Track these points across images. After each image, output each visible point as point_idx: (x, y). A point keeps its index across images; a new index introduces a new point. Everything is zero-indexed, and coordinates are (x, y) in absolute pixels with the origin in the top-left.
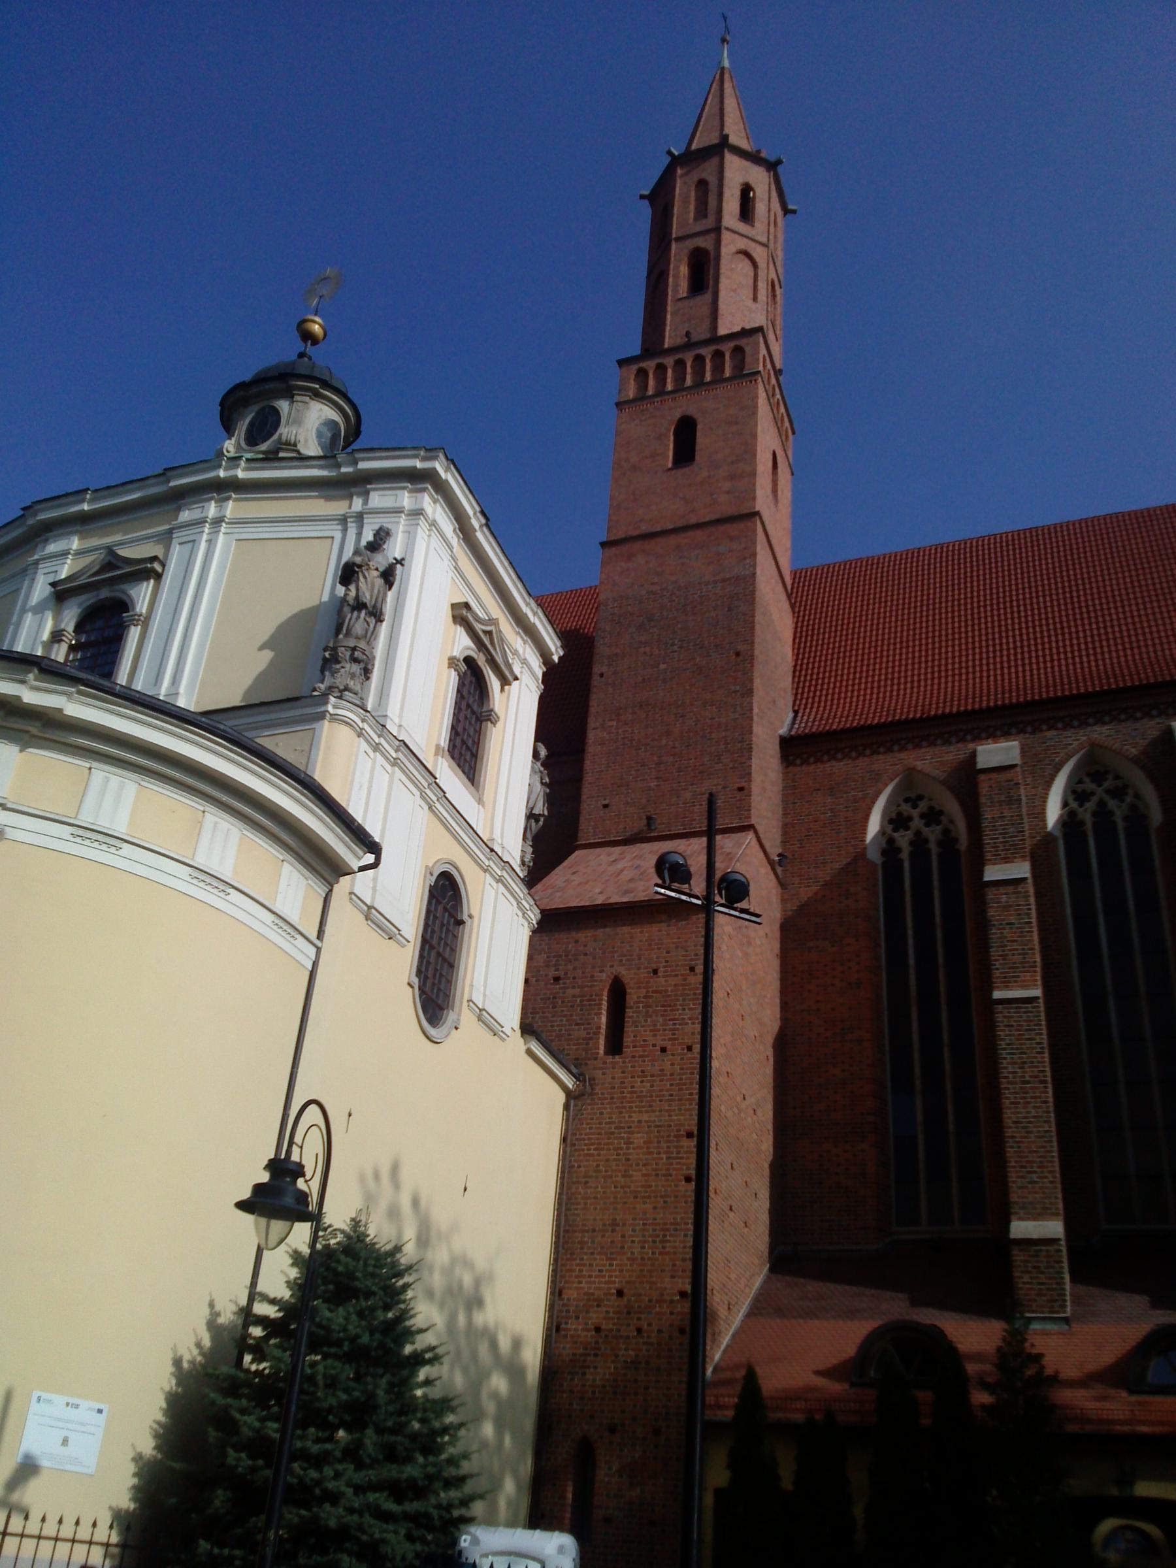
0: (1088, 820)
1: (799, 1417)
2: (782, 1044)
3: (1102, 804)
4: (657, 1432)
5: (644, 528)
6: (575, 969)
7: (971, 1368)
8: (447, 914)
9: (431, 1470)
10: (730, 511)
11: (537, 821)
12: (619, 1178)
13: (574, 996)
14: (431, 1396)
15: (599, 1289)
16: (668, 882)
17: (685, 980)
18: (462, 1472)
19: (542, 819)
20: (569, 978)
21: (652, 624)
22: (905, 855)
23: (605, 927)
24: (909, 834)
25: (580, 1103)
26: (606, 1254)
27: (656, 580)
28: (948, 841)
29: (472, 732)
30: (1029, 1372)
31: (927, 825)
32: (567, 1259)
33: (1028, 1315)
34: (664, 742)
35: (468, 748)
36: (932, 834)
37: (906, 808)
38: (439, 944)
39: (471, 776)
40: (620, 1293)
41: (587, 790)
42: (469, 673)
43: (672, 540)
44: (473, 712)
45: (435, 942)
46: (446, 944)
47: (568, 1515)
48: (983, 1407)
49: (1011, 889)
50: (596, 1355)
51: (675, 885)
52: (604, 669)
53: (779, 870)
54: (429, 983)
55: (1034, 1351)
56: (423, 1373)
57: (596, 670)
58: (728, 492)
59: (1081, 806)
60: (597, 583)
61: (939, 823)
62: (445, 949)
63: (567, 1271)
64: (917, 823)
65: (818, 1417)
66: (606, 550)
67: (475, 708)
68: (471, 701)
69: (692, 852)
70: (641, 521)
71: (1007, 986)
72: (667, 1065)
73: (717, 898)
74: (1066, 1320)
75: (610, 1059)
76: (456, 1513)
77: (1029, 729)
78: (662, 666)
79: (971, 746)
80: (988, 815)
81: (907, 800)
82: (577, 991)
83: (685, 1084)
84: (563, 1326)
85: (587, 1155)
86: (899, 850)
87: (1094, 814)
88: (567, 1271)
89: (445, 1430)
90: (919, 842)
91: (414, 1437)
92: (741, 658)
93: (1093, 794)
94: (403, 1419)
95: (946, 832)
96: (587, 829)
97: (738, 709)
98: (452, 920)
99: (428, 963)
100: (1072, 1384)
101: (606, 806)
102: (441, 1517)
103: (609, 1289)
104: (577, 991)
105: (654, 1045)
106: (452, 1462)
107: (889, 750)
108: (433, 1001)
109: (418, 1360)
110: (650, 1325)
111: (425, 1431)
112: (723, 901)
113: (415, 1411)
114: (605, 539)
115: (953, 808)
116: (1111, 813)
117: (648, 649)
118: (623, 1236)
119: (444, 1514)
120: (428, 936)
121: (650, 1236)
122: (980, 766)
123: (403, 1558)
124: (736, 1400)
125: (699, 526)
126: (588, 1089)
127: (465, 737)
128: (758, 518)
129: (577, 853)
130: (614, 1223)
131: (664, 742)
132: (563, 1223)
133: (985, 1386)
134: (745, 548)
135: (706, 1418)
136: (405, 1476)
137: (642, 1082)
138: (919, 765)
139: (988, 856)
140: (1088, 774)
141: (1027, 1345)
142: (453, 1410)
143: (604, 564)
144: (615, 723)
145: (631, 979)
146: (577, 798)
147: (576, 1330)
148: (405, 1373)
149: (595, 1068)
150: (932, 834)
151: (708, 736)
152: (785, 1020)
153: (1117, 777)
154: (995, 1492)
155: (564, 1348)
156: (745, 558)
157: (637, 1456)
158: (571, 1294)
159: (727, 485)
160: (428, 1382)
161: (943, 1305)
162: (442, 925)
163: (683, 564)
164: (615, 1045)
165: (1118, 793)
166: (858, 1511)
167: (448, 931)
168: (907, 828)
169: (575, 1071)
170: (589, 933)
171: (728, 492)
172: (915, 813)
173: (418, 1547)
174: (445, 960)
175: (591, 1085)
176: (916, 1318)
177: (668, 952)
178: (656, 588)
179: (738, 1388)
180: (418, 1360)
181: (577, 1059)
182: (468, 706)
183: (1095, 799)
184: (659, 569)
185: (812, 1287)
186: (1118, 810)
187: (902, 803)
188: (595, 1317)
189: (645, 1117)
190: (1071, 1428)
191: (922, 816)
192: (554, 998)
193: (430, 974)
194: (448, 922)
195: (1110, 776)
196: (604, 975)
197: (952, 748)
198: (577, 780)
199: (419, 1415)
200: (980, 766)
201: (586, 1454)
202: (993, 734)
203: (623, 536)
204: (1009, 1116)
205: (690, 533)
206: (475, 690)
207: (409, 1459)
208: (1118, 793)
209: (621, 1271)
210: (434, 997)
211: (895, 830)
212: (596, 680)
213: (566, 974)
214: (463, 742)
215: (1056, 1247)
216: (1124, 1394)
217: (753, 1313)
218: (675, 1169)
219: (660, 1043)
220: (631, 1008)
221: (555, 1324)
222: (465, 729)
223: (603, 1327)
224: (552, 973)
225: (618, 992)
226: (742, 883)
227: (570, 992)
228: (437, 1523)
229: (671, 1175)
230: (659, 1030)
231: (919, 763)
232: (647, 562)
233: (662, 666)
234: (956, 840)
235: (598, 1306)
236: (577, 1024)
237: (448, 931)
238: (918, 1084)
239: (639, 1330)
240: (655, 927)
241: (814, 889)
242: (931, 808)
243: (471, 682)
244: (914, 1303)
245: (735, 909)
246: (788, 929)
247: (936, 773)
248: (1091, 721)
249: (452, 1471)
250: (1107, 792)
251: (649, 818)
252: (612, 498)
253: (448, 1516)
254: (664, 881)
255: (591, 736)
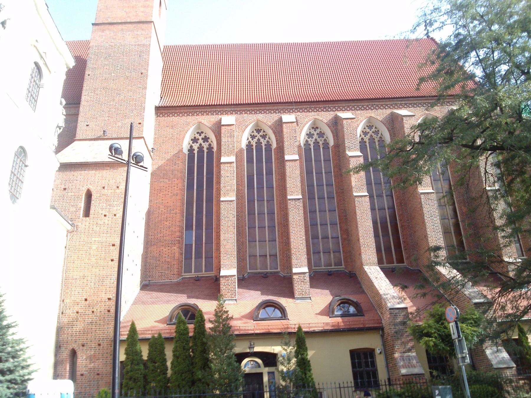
0: (254, 145)
1: (149, 336)
2: (149, 214)
3: (259, 140)
4: (99, 345)
5: (110, 21)
6: (72, 186)
7: (206, 317)
8: (21, 162)
9: (16, 364)
10: (143, 19)
11: (60, 129)
12: (87, 261)
13: (71, 196)
14: (15, 339)
15: (79, 299)
16: (114, 154)
17: (115, 191)
18: (28, 363)
19: (62, 128)
20: (70, 189)
21: (110, 58)
22: (254, 147)
23: (85, 170)
24: (198, 145)
25: (72, 234)
26: (81, 287)
27: (113, 41)
28: (210, 148)
29: (35, 92)
30: (224, 317)
31: (204, 142)
32: (66, 289)
33: (224, 299)
34: (112, 103)
35: (33, 98)
36: (205, 145)
37: (197, 136)
38: (18, 174)
39: (34, 109)
40: (86, 300)
41: (80, 118)
42: (36, 68)
43: (120, 27)
44: (36, 84)
45: (16, 173)
46: (21, 174)
47: (68, 375)
48: (210, 328)
49: (229, 165)
50: (77, 321)
51: (116, 156)
52: (90, 73)
53: (152, 154)
54: (13, 188)
55: (226, 310)
56: (11, 331)
57: (87, 73)
58: (142, 12)
59: (252, 140)
60: (90, 39)
61: (208, 142)
62: (20, 176)
63: (66, 293)
64: (200, 141)
65: (156, 336)
66: (94, 27)
67: (37, 82)
68: (36, 79)
69: (124, 145)
70: (109, 17)
71: (225, 196)
72: (106, 222)
73: (132, 161)
74: (236, 300)
75: (84, 218)
76: (26, 377)
77: (239, 113)
78: (113, 74)
79: (220, 116)
80: (224, 140)
81: (198, 133)
82: (73, 194)
83: (113, 228)
84: (64, 312)
85: (74, 253)
86: (194, 150)
87: (256, 143)
88: (66, 293)
89: (21, 350)
90: (201, 148)
91: (9, 353)
92: (143, 75)
93: (256, 136)
94: (4, 347)
95: (210, 145)
96: (79, 134)
97: (141, 94)
98: (23, 165)
99: (13, 181)
100: (237, 319)
101: (87, 125)
102: (21, 380)
103: (82, 298)
104: (73, 194)
105: (102, 214)
106: (24, 360)
107: (193, 115)
108: (14, 195)
109: (8, 327)
110: (97, 310)
111: (13, 350)
112: (134, 162)
113: (8, 344)
114: (94, 22)
115: (212, 138)
116: (261, 143)
117: (108, 67)
118: (87, 280)
119: (21, 378)
120: (13, 171)
121: (97, 280)
122: (222, 124)
123: (6, 395)
124: (128, 332)
125: (131, 23)
126: (76, 229)
127: (32, 94)
128: (153, 23)
129: (75, 142)
130: (84, 277)
131: (112, 103)
132: (64, 277)
133: (211, 321)
134: (147, 34)
135: (121, 339)
136: (6, 367)
137: (96, 227)
138: (203, 121)
139: (222, 154)
140: (255, 130)
141: (224, 308)
142: (24, 343)
143: (93, 32)
144: (93, 94)
145: (94, 190)
146: (76, 121)
147: (69, 313)
148: (4, 331)
149: (78, 222)
150: (205, 145)
151: (129, 102)
152: (150, 206)
153: (264, 132)
154: (212, 354)
155: (65, 320)
156: (147, 38)
157: (92, 353)
158: (67, 301)
159: (142, 9)
160: (13, 334)
161: (197, 298)
162: (19, 166)
163: (124, 36)
164: (87, 213)
165: (264, 137)
166: (169, 364)
167: (22, 169)
168: (197, 143)
169: (70, 223)
170: (79, 173)
171: (142, 12)
172: (200, 138)
173: (12, 391)
174: (20, 180)
175: (76, 228)
176: (189, 302)
177: (109, 181)
178: (112, 44)
179: (129, 329)
180: (8, 327)
181: (71, 219)
182: (34, 81)
183: (257, 138)
184: (114, 37)
185: (155, 294)
186: (264, 142)
187: (196, 134)
188: (76, 308)
189: (97, 239)
190: (236, 333)
191: (202, 139)
192: (64, 196)
193: (14, 185)
194: (22, 166)
195: (262, 131)
196: (84, 188)
197: (214, 116)
198: (77, 115)
199: (11, 345)
200: (222, 124)
201: (74, 353)
202: (289, 112)
203: (101, 22)
204: (222, 237)
205: (127, 25)
206: (38, 75)
207: (7, 361)
208: (264, 137)
209: (86, 292)
210: (15, 194)
211: (193, 143)
212: (86, 76)
213: (69, 187)
214: (32, 95)
215: (234, 278)
216: (252, 321)
217: (134, 303)
218: (108, 257)
219: (104, 213)
220: (94, 200)
221: (61, 312)
222: (32, 90)
223: (80, 311)
224: (63, 187)
225: (89, 196)
226: (142, 156)
227: (70, 194)
228: (19, 382)
229: (106, 259)
230: (104, 209)
231: (203, 120)
232: (110, 34)
233: (113, 74)
234: (213, 148)
235: (77, 305)
236: (72, 206)
237: (22, 169)
238: (194, 227)
239: (93, 312)
240: (105, 172)
241: (164, 161)
242: (206, 136)
243: (36, 72)
244: (189, 297)
245: (138, 165)
246: (153, 175)
247: (208, 124)
248: (258, 112)
249: (24, 364)
250: (261, 136)
251: (104, 131)
252: (98, 7)
253: (23, 379)
254: (112, 154)
255: (83, 98)
